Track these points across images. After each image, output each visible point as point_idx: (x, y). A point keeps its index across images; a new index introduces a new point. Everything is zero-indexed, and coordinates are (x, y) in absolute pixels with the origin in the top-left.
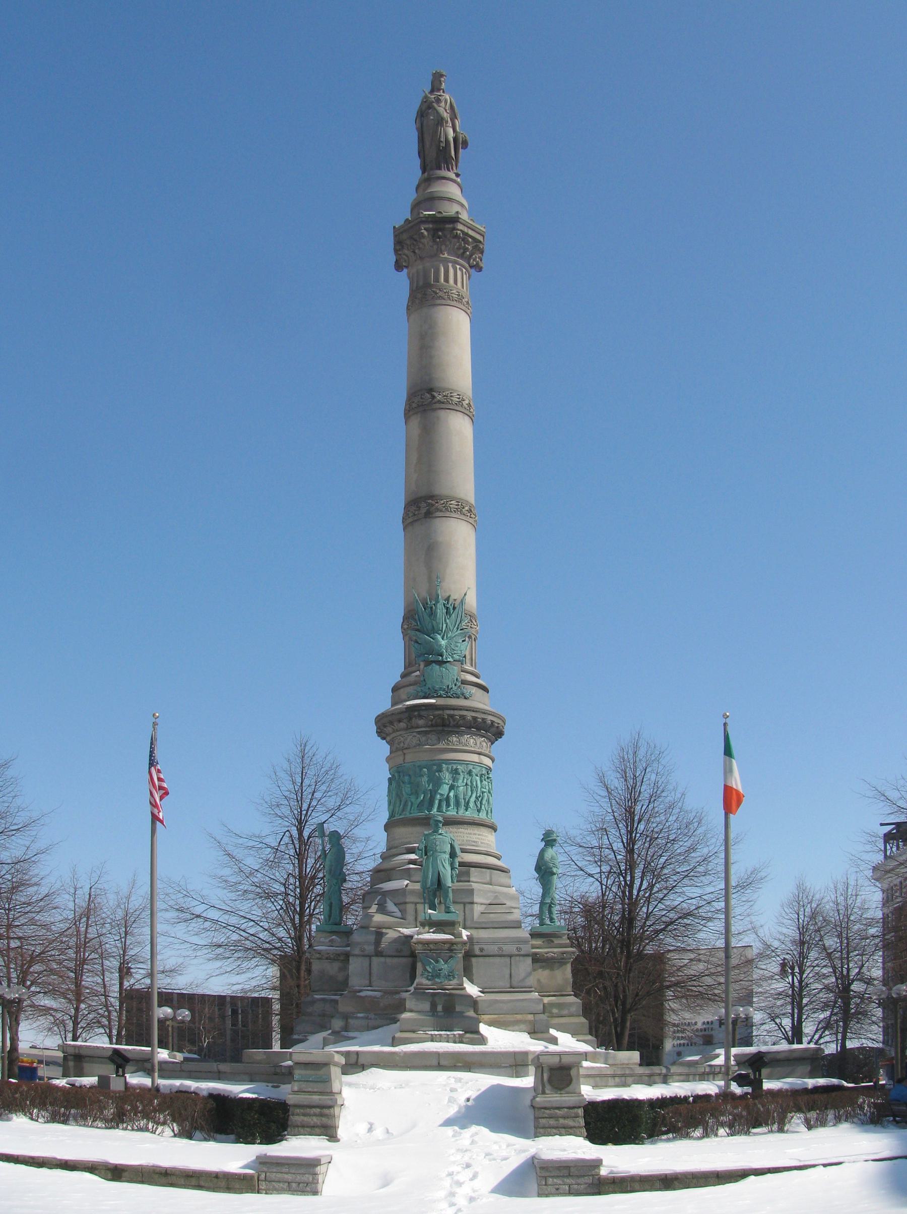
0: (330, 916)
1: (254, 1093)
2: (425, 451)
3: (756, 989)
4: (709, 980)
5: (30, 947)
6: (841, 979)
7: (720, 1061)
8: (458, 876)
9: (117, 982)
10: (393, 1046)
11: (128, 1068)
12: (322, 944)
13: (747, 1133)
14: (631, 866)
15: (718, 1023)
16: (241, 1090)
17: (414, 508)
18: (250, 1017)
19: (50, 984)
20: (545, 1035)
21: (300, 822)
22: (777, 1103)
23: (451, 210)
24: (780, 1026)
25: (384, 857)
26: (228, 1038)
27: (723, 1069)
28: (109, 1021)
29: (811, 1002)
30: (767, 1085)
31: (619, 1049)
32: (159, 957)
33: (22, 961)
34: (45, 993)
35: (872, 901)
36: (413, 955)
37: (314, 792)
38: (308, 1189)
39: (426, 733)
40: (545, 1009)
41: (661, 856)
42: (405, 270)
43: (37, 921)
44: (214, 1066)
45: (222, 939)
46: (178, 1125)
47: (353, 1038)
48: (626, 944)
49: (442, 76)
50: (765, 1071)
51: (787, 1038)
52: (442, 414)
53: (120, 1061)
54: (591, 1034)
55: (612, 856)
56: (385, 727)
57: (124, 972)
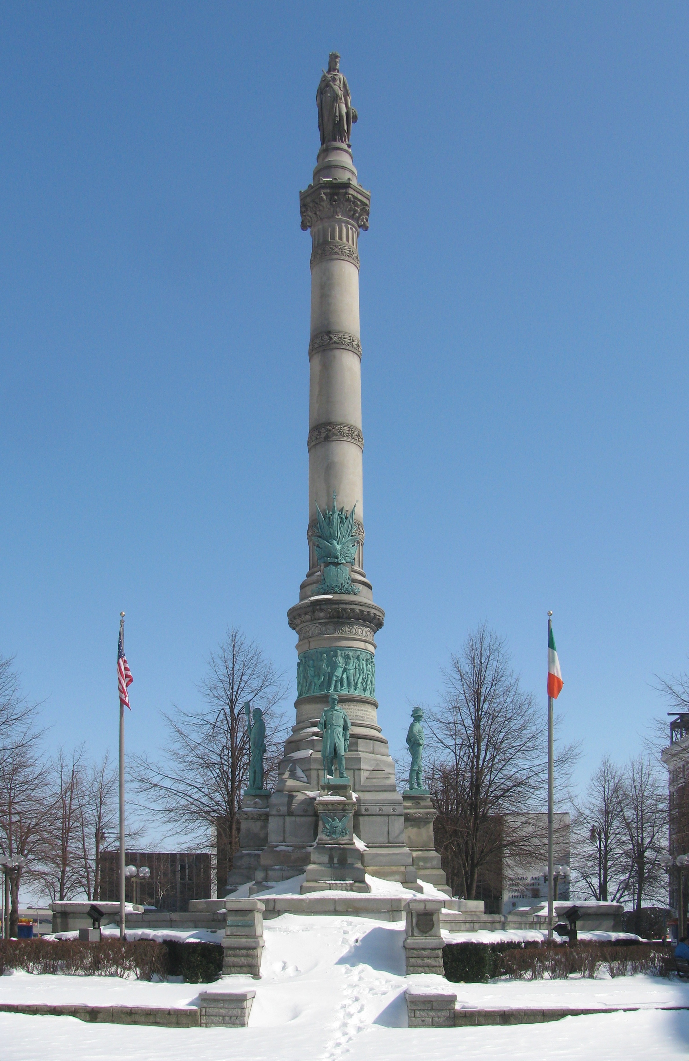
0: (254, 782)
1: (197, 938)
2: (324, 385)
3: (573, 851)
4: (536, 841)
5: (27, 820)
6: (637, 846)
7: (544, 912)
8: (349, 746)
9: (94, 846)
10: (301, 894)
11: (103, 921)
12: (249, 806)
13: (566, 977)
14: (478, 739)
15: (542, 879)
16: (187, 936)
17: (316, 433)
18: (194, 871)
19: (42, 852)
20: (413, 885)
21: (232, 702)
22: (588, 952)
23: (344, 177)
24: (590, 884)
25: (295, 730)
26: (178, 890)
27: (547, 920)
28: (88, 880)
29: (614, 865)
30: (582, 936)
31: (469, 898)
32: (126, 823)
33: (21, 833)
34: (39, 859)
35: (660, 780)
36: (316, 815)
37: (242, 675)
38: (238, 1022)
39: (325, 624)
40: (414, 862)
41: (500, 732)
42: (309, 230)
43: (32, 797)
44: (167, 915)
45: (173, 805)
46: (140, 969)
47: (272, 887)
48: (474, 806)
49: (337, 57)
50: (579, 923)
51: (595, 896)
52: (337, 352)
53: (96, 915)
54: (448, 885)
55: (463, 731)
56: (295, 619)
57: (100, 837)
